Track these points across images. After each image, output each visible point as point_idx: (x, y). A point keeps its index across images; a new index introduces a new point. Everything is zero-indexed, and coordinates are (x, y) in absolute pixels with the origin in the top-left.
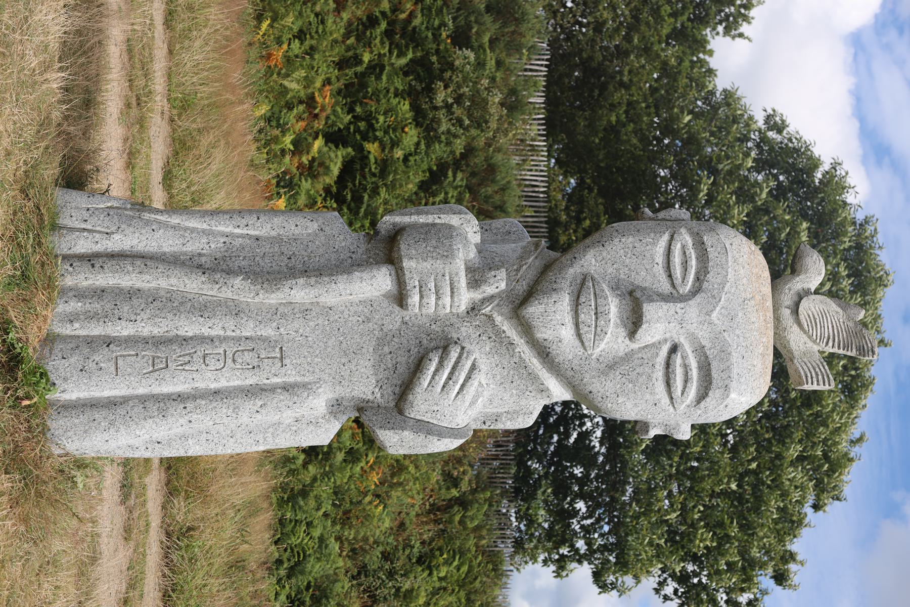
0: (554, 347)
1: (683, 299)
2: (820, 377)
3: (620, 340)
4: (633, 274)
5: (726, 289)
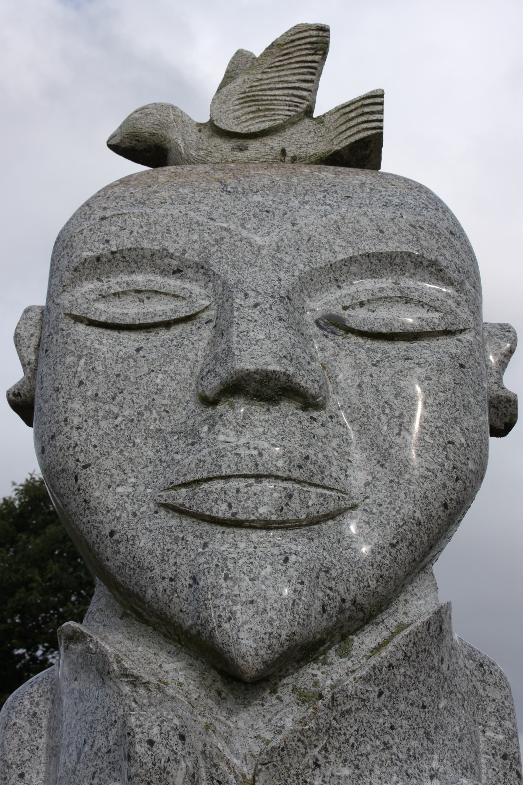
0: (341, 588)
1: (224, 295)
2: (366, 110)
3: (321, 432)
4: (159, 400)
5: (201, 219)
